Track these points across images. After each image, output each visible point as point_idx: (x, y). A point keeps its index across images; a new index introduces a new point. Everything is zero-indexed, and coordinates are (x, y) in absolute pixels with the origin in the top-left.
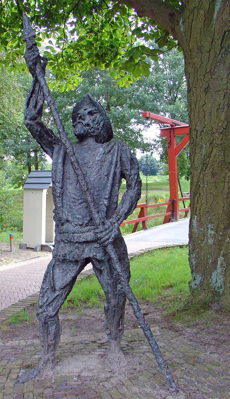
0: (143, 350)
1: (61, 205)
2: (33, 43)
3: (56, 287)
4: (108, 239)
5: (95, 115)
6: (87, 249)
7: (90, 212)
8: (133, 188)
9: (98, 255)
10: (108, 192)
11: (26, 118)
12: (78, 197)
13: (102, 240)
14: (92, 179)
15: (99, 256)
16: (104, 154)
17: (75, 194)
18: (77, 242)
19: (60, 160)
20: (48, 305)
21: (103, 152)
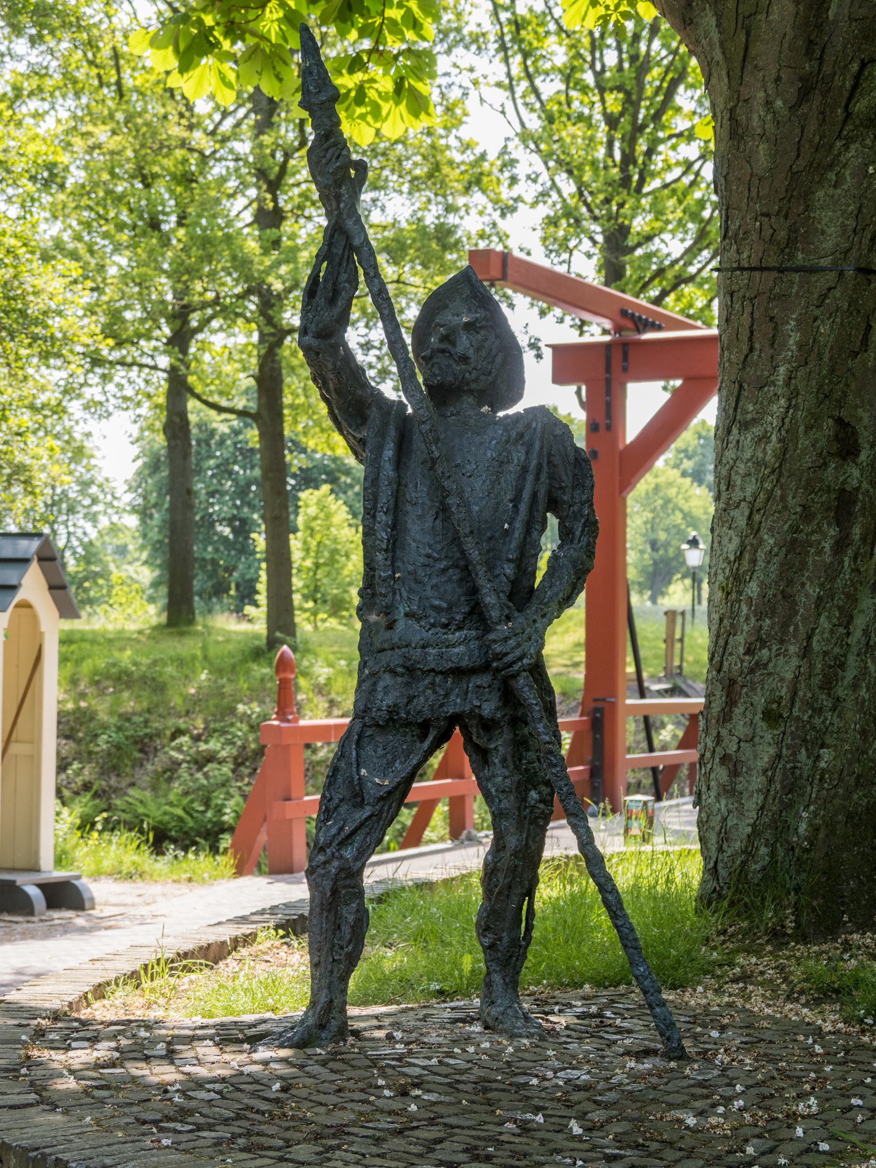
0: (238, 1123)
3: (366, 797)
4: (520, 658)
5: (483, 332)
7: (474, 591)
9: (485, 706)
10: (513, 545)
12: (439, 552)
13: (507, 659)
14: (476, 508)
15: (489, 708)
16: (507, 442)
17: (430, 546)
18: (433, 670)
19: (389, 453)
20: (343, 844)
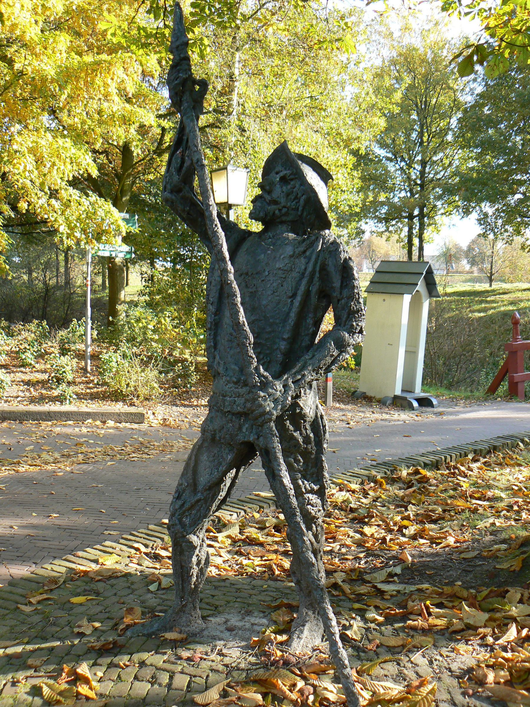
1: (212, 344)
2: (182, 56)
5: (292, 183)
6: (247, 426)
8: (343, 323)
11: (165, 188)
21: (292, 253)
